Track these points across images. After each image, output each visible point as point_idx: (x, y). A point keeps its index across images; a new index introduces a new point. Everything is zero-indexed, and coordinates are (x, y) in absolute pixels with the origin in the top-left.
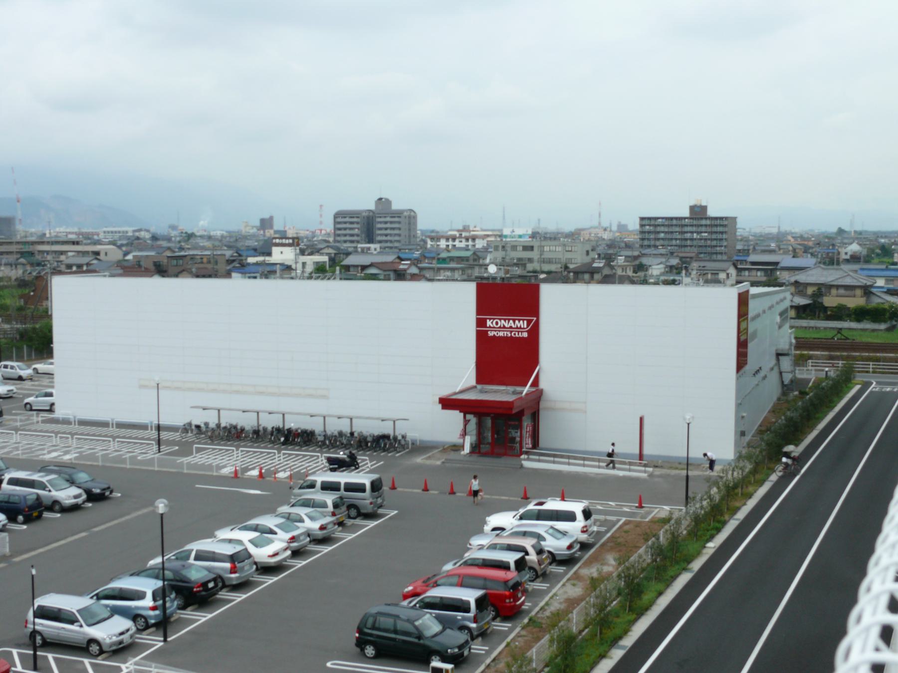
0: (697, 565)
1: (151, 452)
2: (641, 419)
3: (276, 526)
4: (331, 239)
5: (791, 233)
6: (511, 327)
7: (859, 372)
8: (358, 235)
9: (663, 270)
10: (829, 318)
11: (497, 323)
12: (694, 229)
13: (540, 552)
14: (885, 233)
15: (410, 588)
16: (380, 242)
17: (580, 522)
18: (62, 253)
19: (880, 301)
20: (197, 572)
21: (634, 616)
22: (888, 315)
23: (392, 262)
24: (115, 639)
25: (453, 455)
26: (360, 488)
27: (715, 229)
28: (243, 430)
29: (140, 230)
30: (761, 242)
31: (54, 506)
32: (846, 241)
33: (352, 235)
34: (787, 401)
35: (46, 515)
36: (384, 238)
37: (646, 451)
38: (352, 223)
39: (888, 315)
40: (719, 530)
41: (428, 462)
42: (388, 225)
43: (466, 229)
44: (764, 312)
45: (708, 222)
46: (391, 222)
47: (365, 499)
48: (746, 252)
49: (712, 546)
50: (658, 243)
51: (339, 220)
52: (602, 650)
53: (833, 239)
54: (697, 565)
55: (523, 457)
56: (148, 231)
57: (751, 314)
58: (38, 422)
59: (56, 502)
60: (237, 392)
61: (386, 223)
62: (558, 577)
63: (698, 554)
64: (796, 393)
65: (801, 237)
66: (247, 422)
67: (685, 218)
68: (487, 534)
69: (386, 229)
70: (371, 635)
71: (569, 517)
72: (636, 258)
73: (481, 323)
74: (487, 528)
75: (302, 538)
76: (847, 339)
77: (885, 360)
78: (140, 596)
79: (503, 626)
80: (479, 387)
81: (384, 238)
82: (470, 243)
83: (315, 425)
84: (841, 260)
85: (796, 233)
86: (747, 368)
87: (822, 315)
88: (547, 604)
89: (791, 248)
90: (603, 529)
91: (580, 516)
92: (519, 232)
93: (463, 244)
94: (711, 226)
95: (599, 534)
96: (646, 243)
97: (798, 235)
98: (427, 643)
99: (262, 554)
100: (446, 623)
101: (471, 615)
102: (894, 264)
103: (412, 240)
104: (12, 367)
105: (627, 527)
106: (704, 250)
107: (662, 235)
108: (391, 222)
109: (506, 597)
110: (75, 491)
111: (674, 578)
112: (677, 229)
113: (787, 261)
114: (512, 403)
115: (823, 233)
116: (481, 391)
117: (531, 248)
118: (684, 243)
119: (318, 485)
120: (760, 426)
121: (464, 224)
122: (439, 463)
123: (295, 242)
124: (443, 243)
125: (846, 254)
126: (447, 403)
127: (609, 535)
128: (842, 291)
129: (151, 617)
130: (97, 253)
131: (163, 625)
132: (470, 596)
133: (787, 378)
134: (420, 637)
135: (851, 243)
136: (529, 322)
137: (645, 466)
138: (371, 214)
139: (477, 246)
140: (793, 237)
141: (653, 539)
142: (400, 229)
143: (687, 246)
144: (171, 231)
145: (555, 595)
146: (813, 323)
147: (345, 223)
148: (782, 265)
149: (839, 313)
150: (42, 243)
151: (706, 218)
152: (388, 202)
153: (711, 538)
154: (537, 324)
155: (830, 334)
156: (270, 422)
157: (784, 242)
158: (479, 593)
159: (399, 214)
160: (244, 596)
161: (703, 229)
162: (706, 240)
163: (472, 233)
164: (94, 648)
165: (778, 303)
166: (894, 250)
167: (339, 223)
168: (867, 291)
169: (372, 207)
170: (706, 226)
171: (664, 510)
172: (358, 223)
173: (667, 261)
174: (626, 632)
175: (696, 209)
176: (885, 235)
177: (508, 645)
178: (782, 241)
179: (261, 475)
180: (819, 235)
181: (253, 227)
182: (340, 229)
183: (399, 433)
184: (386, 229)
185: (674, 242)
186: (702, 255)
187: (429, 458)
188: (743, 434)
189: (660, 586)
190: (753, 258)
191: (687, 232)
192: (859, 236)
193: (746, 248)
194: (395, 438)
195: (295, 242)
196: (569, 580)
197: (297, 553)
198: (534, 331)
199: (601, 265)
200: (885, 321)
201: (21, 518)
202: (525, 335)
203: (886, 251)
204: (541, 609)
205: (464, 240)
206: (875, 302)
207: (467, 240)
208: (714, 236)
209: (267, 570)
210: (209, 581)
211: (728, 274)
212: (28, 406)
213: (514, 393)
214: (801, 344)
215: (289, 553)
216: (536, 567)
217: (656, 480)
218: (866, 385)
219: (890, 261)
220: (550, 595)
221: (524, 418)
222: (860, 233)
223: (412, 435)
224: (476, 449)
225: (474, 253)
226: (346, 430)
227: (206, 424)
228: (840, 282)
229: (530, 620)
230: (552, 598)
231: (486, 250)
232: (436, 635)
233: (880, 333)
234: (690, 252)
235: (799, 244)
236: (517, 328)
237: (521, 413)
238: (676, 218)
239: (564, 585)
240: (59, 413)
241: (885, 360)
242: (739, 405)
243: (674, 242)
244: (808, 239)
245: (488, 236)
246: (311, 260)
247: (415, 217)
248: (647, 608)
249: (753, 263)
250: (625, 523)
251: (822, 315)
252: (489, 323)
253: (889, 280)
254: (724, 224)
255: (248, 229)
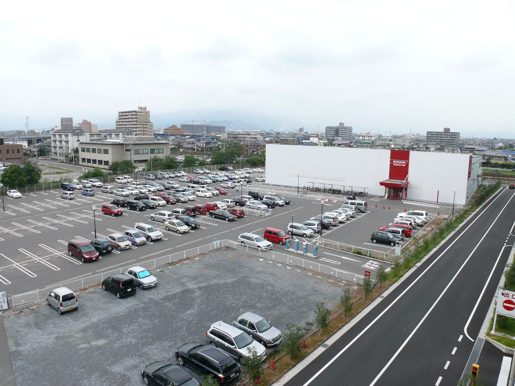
0: (457, 229)
1: (296, 194)
2: (438, 191)
3: (342, 212)
4: (324, 135)
5: (477, 139)
6: (400, 163)
7: (502, 183)
8: (333, 134)
9: (434, 149)
10: (492, 167)
11: (396, 162)
12: (445, 136)
13: (415, 222)
14: (511, 140)
15: (382, 228)
16: (340, 137)
17: (425, 216)
18: (245, 138)
19: (510, 162)
20: (326, 221)
21: (441, 239)
22: (512, 167)
23: (348, 143)
24: (310, 234)
25: (381, 199)
26: (361, 205)
27: (452, 136)
28: (320, 189)
29: (263, 131)
30: (467, 141)
31: (278, 205)
32: (497, 142)
33: (331, 134)
34: (480, 190)
35: (276, 207)
36: (341, 136)
37: (438, 201)
38: (332, 130)
39: (512, 167)
40: (462, 222)
41: (375, 200)
42: (343, 132)
43: (368, 133)
44: (476, 162)
45: (450, 134)
46: (344, 131)
47: (362, 208)
48: (462, 144)
49: (461, 225)
50: (432, 140)
51: (327, 129)
52: (434, 245)
53: (492, 141)
54: (457, 229)
55: (403, 200)
56: (265, 131)
57: (472, 163)
58: (261, 184)
59: (278, 204)
60: (318, 178)
61: (342, 131)
62: (419, 230)
63: (457, 227)
64: (482, 188)
65: (481, 140)
66: (322, 187)
67: (442, 132)
68: (398, 218)
69: (342, 133)
70: (375, 237)
71: (422, 214)
72: (426, 145)
73: (391, 161)
74: (398, 216)
75: (348, 215)
76: (499, 173)
77: (511, 180)
78: (314, 225)
79: (408, 239)
80: (390, 180)
81: (341, 136)
82: (370, 138)
83: (342, 189)
84: (495, 148)
85: (479, 139)
86: (470, 178)
87: (490, 166)
88: (418, 235)
89: (478, 144)
90: (429, 219)
91: (425, 214)
92: (388, 135)
93: (367, 138)
94: (451, 135)
95: (429, 221)
96: (428, 140)
97: (480, 139)
98: (390, 240)
99: (340, 218)
100: (395, 236)
101: (400, 234)
102: (514, 150)
103: (351, 136)
104: (247, 170)
105: (436, 219)
106: (448, 143)
107: (434, 138)
108: (344, 131)
109: (408, 231)
110: (282, 201)
111: (451, 232)
112: (439, 136)
113: (478, 148)
114: (401, 184)
115: (489, 139)
116: (391, 181)
117: (392, 140)
118: (441, 141)
119: (349, 203)
120: (472, 196)
121: (368, 132)
122: (378, 200)
123: (317, 136)
124: (361, 138)
125: (497, 146)
126: (382, 184)
127: (431, 221)
128: (497, 158)
129: (317, 230)
130: (256, 138)
131: (320, 232)
132: (400, 230)
133: (480, 183)
134: (388, 238)
135: (499, 143)
136: (406, 162)
137: (439, 205)
138: (338, 128)
139: (372, 139)
140: (478, 140)
141: (446, 221)
142: (347, 133)
143: (442, 142)
144: (271, 131)
145: (419, 233)
146: (486, 168)
147: (329, 130)
148: (476, 149)
149: (496, 165)
150: (240, 134)
151: (450, 133)
152: (343, 124)
153: (460, 223)
154: (408, 162)
155: (493, 172)
156: (328, 187)
157: (476, 142)
158: (402, 229)
159: (347, 128)
160: (337, 228)
161: (448, 136)
162: (449, 140)
163: (370, 135)
164: (305, 236)
165: (479, 160)
166: (514, 146)
167: (327, 130)
168: (506, 158)
169: (338, 126)
170: (449, 135)
171: (446, 216)
172: (333, 131)
173: (436, 146)
174: (440, 242)
175: (446, 129)
176: (511, 140)
177: (409, 242)
178: (475, 141)
179: (329, 201)
180: (487, 140)
181: (297, 131)
182: (327, 132)
183: (366, 192)
184: (342, 133)
185: (438, 140)
186: (447, 145)
187: (375, 199)
188: (468, 198)
189: (448, 233)
190: (466, 146)
191: (443, 137)
192: (502, 141)
193: (463, 143)
194: (365, 193)
195: (317, 136)
196: (422, 230)
197: (347, 220)
198: (407, 165)
199: (416, 147)
200: (511, 169)
201: (270, 207)
202: (404, 165)
203: (511, 146)
204: (416, 236)
205: (368, 137)
206: (508, 162)
207: (369, 137)
208: (452, 139)
209: (341, 222)
210: (329, 223)
211: (458, 151)
212: (256, 180)
213: (401, 182)
214: (484, 174)
215: (346, 219)
216: (414, 226)
217: (442, 209)
218: (505, 188)
219: (513, 149)
220: (418, 233)
221: (403, 189)
222: (502, 140)
223: (370, 193)
224: (389, 197)
225: (372, 141)
226: (350, 190)
227: (310, 187)
228: (497, 155)
229: (414, 238)
230: (419, 233)
231: (375, 140)
232: (392, 238)
233: (509, 172)
234: (444, 144)
235: (481, 143)
236: (402, 163)
237: (403, 188)
238: (439, 132)
239: (421, 231)
240: (266, 182)
241: (511, 180)
242: (467, 189)
243: (438, 140)
244: (484, 141)
245: (375, 136)
246: (322, 142)
247: (352, 129)
248: (444, 238)
249: (466, 148)
250: (435, 218)
251: (490, 166)
252: (394, 162)
253: (513, 155)
254: (455, 135)
255: (295, 131)
